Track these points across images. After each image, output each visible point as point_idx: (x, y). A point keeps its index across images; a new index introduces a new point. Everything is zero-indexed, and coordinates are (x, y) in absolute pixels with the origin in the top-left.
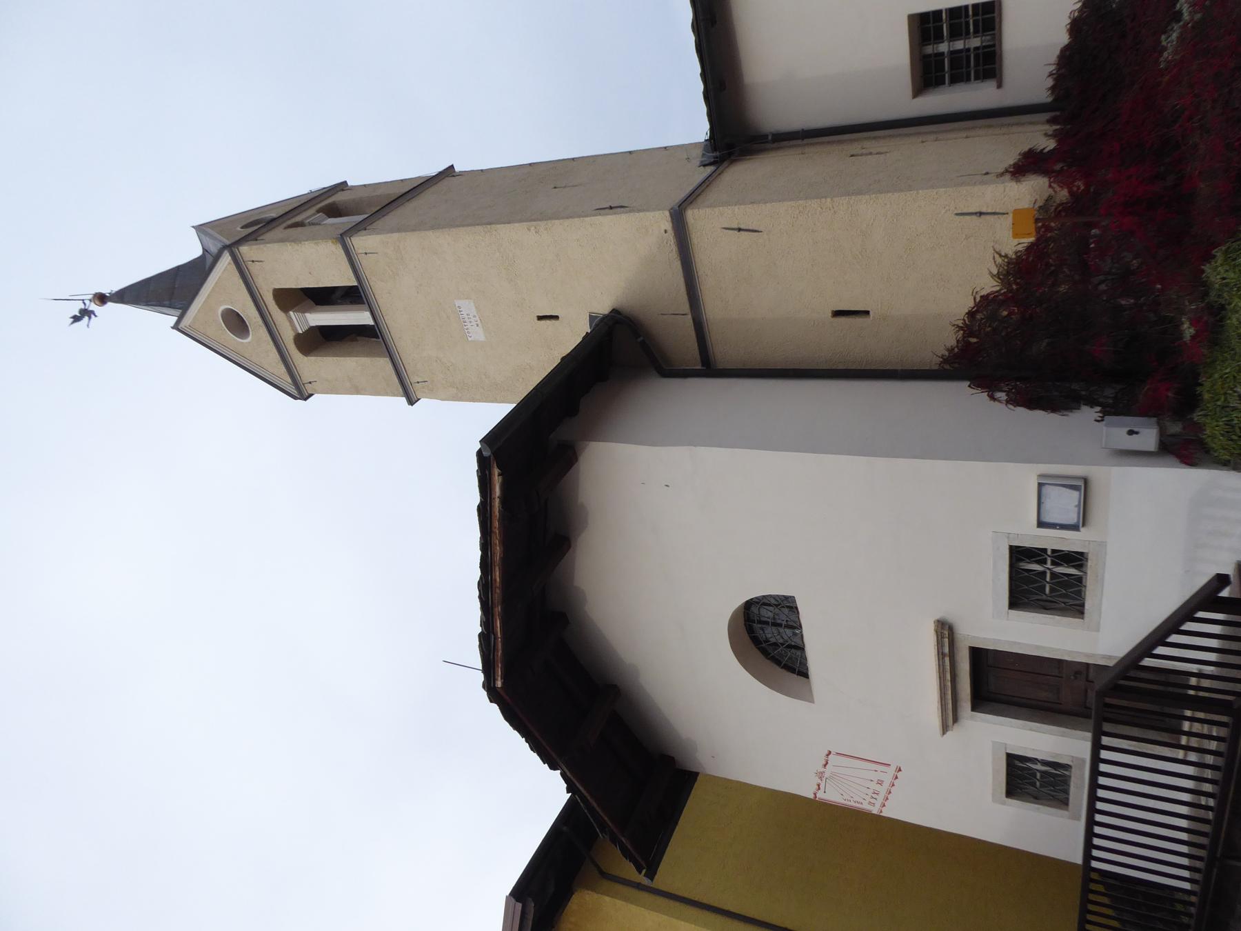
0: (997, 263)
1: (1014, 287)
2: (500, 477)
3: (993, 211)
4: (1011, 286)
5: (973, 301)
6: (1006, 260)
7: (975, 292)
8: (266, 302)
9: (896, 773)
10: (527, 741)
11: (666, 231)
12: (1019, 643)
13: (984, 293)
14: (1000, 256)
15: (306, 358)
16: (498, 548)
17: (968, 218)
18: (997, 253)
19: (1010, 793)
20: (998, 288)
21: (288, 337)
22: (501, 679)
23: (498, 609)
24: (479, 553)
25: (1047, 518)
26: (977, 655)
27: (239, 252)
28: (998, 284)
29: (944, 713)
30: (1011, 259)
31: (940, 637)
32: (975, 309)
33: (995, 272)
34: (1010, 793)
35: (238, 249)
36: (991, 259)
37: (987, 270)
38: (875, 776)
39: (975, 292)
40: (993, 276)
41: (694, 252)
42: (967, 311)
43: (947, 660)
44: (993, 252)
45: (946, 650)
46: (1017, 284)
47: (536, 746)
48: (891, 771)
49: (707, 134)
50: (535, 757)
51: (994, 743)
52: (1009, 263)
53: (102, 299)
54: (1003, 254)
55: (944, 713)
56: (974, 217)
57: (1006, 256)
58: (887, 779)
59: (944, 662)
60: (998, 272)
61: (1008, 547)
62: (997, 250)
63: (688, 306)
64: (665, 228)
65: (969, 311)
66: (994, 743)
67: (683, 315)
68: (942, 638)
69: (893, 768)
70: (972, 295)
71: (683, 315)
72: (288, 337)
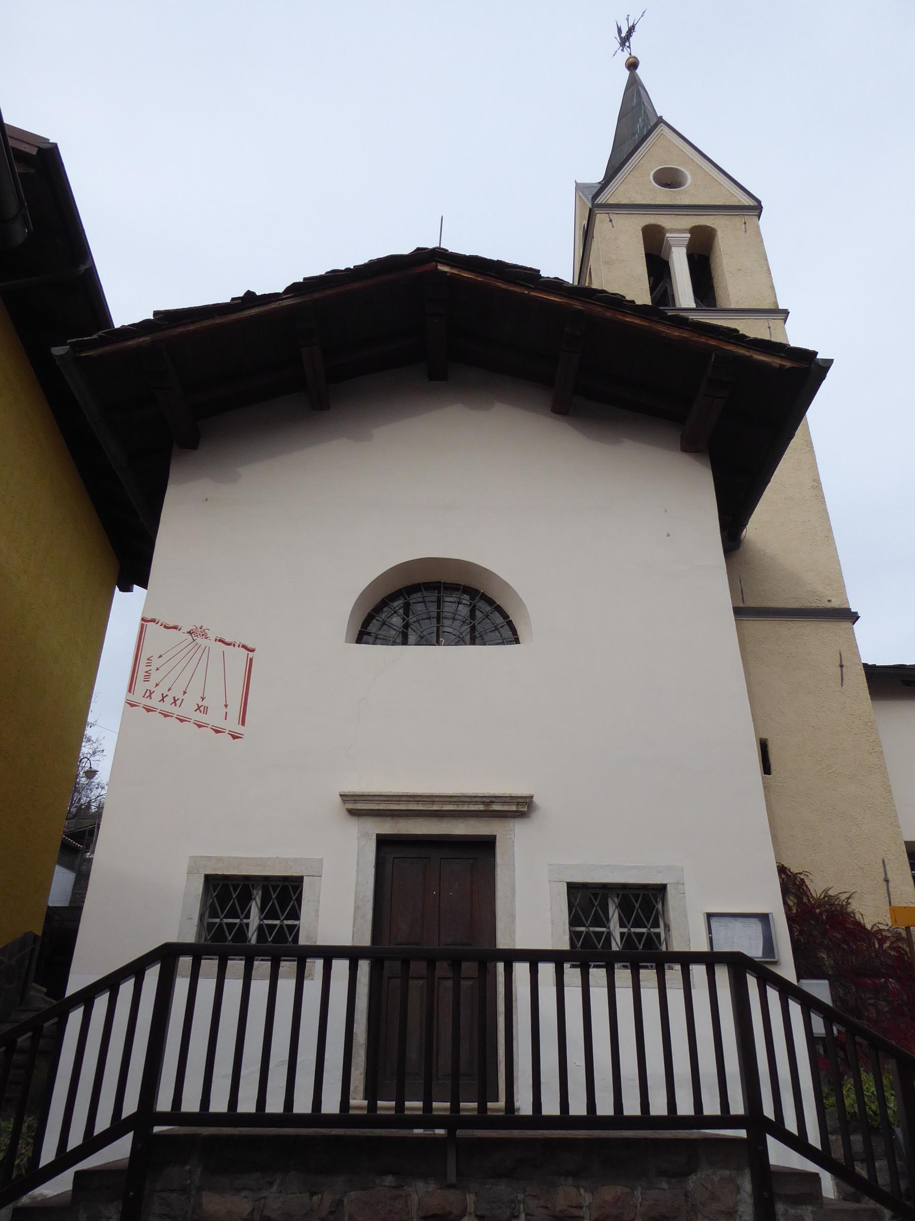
0: (840, 895)
1: (818, 911)
2: (779, 365)
3: (891, 893)
4: (818, 908)
5: (798, 872)
6: (844, 903)
7: (807, 874)
8: (700, 217)
9: (227, 732)
10: (348, 270)
11: (830, 601)
12: (514, 894)
13: (807, 882)
14: (848, 898)
15: (641, 228)
16: (677, 334)
17: (882, 870)
18: (851, 895)
19: (210, 880)
20: (814, 895)
21: (665, 221)
22: (452, 273)
23: (578, 306)
24: (227, 299)
25: (714, 923)
26: (487, 845)
27: (754, 215)
28: (818, 895)
29: (384, 799)
30: (846, 908)
31: (520, 800)
32: (790, 874)
33: (831, 893)
34: (210, 880)
35: (756, 215)
36: (844, 890)
37: (831, 885)
38: (214, 702)
39: (807, 874)
40: (826, 891)
41: (828, 623)
42: (786, 866)
43: (481, 807)
44: (852, 892)
45: (496, 807)
46: (821, 913)
47: (334, 278)
48: (233, 724)
49: (92, 711)
50: (319, 270)
51: (321, 861)
52: (842, 906)
53: (632, 65)
54: (850, 901)
55: (384, 799)
56: (883, 875)
57: (848, 904)
58: (214, 718)
59: (476, 803)
60: (830, 896)
61: (664, 882)
62: (853, 896)
63: (753, 605)
64: (832, 601)
65: (786, 868)
66: (321, 861)
67: (743, 599)
68: (518, 804)
69: (239, 729)
70: (803, 871)
71: (743, 599)
72: (665, 221)
